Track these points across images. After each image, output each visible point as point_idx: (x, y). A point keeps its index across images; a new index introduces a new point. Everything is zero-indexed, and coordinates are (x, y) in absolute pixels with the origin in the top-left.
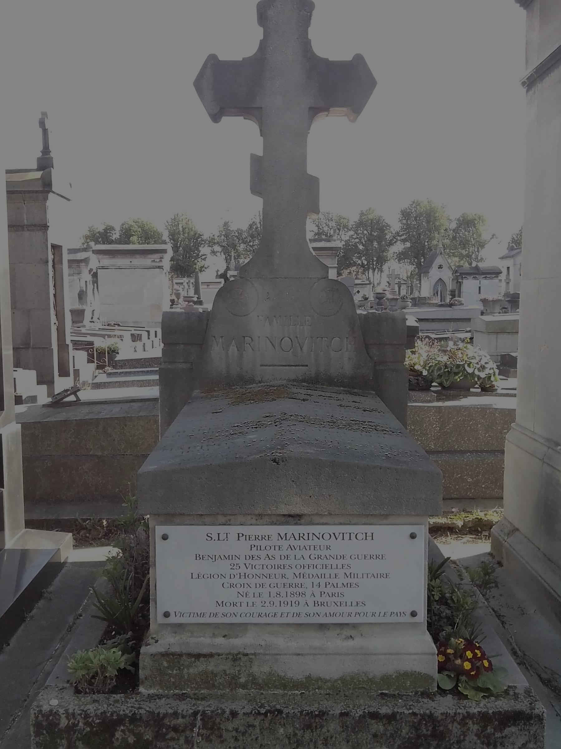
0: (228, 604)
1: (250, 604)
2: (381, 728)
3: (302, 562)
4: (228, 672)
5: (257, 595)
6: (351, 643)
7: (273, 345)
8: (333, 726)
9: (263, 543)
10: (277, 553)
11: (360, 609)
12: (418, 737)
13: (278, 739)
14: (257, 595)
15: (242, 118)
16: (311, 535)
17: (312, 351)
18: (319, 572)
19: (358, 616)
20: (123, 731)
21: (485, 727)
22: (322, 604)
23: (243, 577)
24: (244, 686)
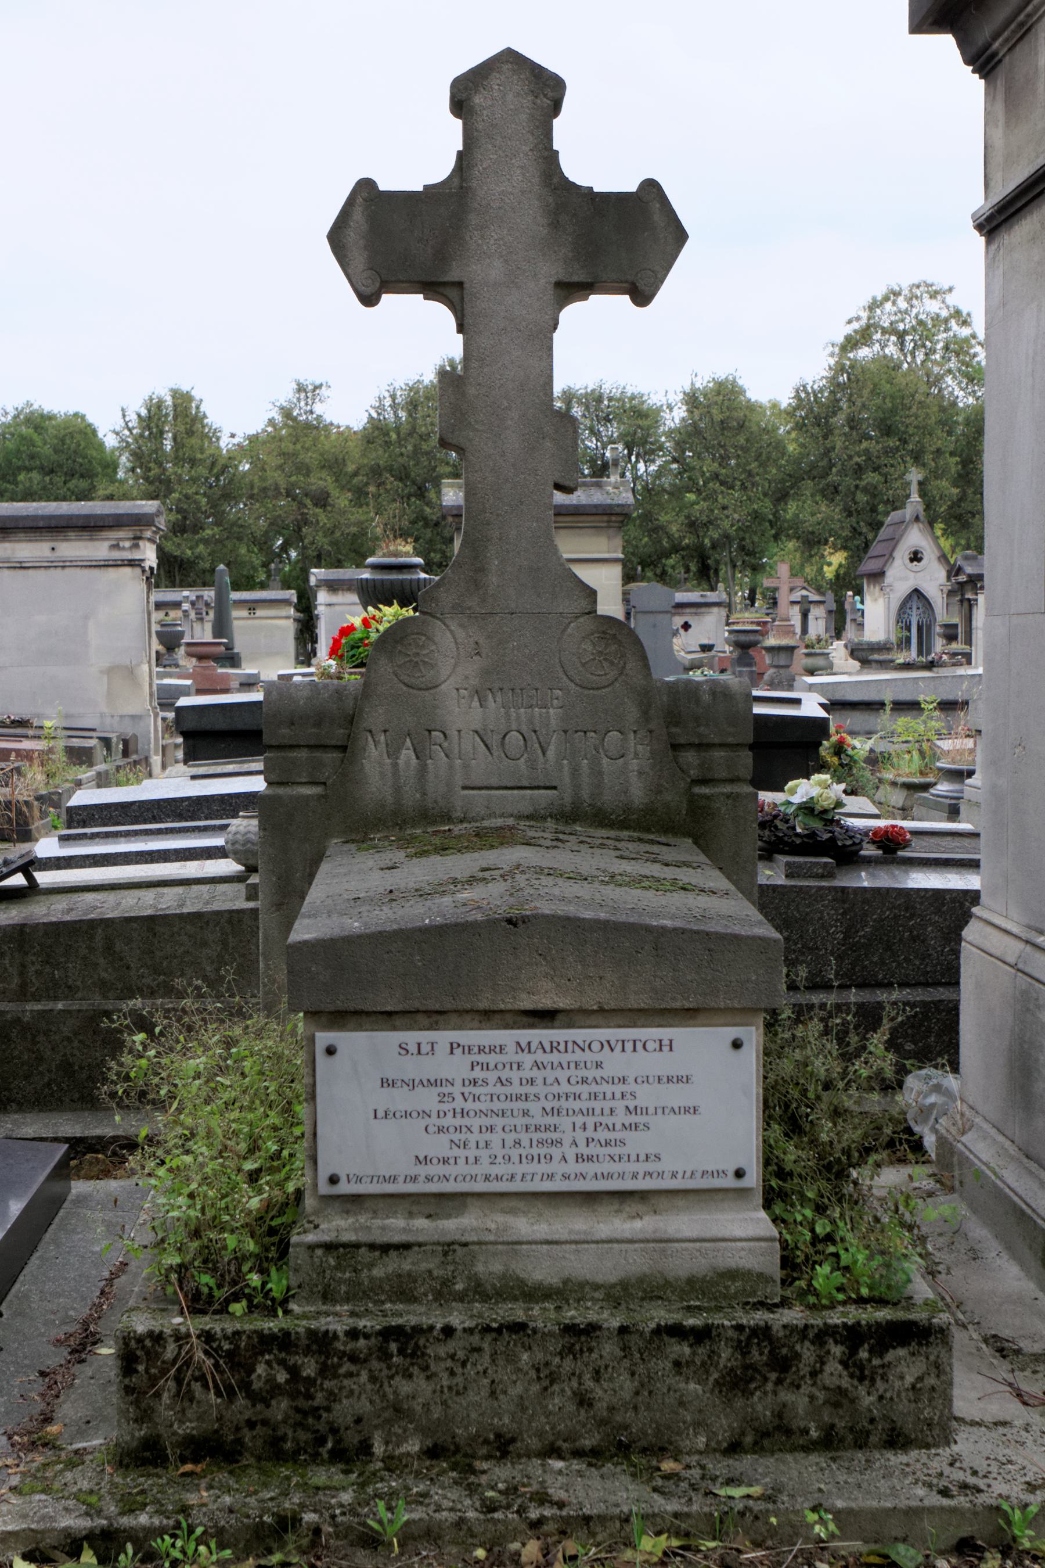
0: (435, 1161)
1: (471, 1160)
2: (687, 1350)
3: (555, 1089)
4: (435, 1273)
5: (482, 1144)
6: (638, 1224)
7: (486, 746)
8: (609, 1349)
9: (492, 1059)
10: (515, 1075)
11: (651, 1167)
12: (746, 1367)
13: (520, 1370)
14: (482, 1144)
15: (421, 296)
16: (570, 1045)
17: (564, 758)
18: (584, 1105)
19: (648, 1177)
20: (268, 1363)
21: (853, 1350)
22: (590, 1159)
23: (459, 1116)
24: (461, 1297)
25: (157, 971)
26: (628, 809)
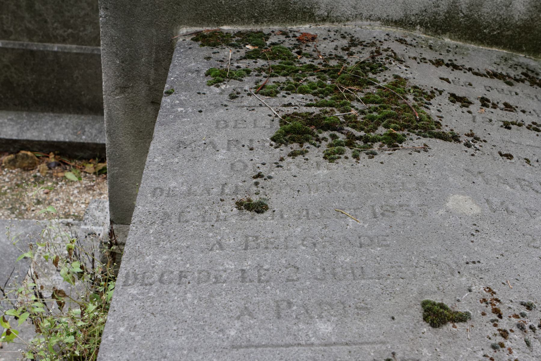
25: (66, 25)
26: (504, 24)
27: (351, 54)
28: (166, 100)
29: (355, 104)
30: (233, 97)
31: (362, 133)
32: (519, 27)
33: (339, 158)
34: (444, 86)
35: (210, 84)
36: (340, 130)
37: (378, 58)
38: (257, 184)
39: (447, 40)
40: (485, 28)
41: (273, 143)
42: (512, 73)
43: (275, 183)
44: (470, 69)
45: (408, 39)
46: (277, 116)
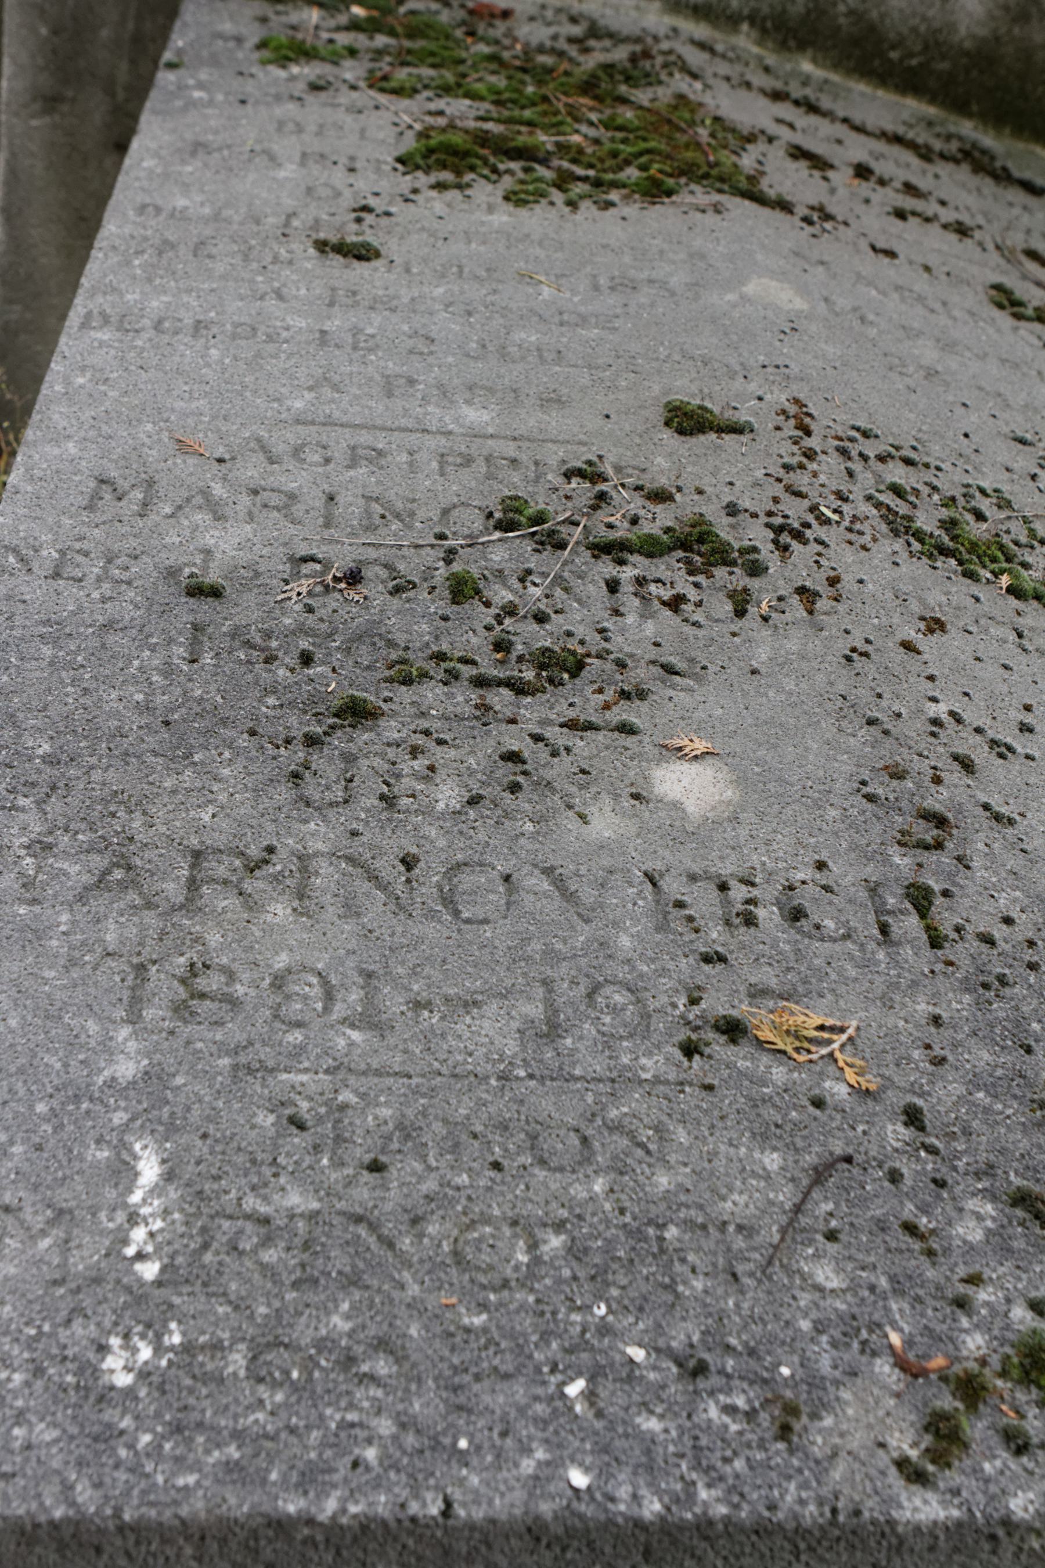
26: (935, 43)
27: (586, 50)
28: (165, 78)
29: (584, 128)
30: (315, 87)
31: (591, 173)
32: (967, 54)
33: (537, 202)
34: (784, 132)
35: (264, 63)
36: (544, 162)
37: (647, 64)
38: (359, 220)
39: (807, 67)
40: (893, 47)
41: (399, 166)
42: (937, 145)
43: (397, 224)
44: (845, 120)
45: (720, 48)
46: (410, 127)
